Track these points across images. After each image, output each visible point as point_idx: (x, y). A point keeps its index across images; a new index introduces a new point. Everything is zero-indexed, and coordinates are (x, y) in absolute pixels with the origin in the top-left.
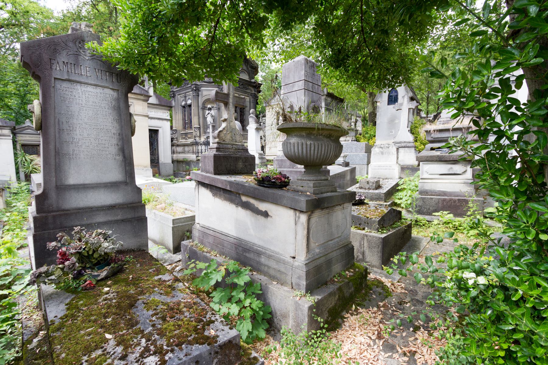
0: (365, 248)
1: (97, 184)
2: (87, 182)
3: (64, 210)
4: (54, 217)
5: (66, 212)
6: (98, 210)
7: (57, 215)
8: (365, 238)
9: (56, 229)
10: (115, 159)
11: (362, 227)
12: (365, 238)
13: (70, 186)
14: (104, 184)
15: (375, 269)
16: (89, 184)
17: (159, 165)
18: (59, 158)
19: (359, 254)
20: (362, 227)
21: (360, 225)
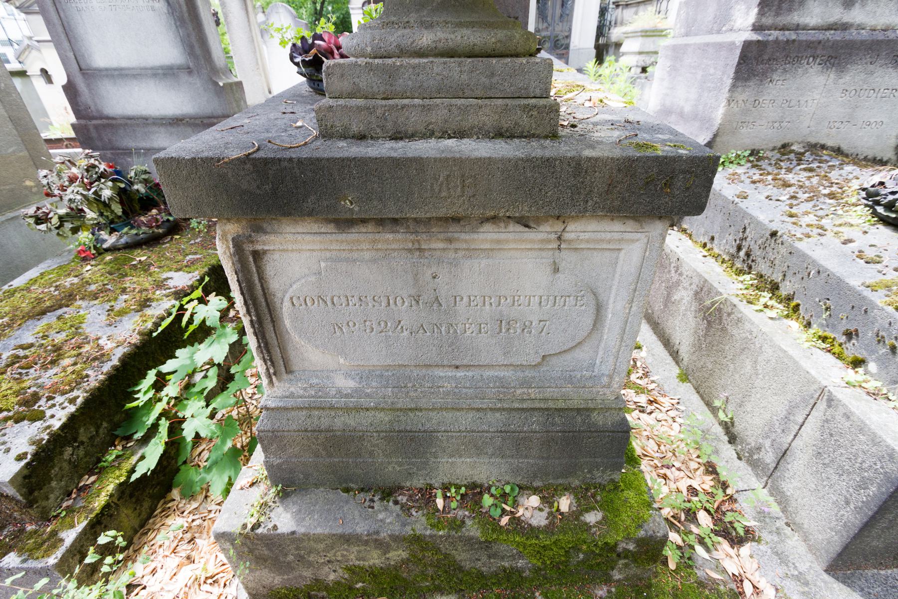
0: (798, 443)
1: (141, 69)
2: (124, 64)
3: (108, 118)
4: (96, 127)
5: (111, 122)
6: (154, 124)
7: (99, 125)
8: (822, 405)
9: (107, 150)
10: (153, 9)
11: (853, 350)
12: (822, 405)
13: (100, 70)
14: (152, 68)
15: (794, 543)
16: (129, 69)
17: (568, 53)
18: (63, 10)
19: (767, 443)
20: (853, 350)
21: (849, 335)
